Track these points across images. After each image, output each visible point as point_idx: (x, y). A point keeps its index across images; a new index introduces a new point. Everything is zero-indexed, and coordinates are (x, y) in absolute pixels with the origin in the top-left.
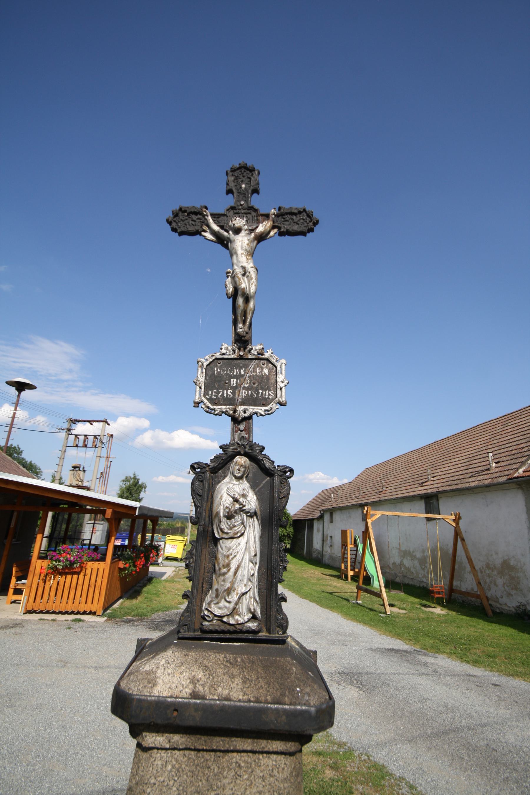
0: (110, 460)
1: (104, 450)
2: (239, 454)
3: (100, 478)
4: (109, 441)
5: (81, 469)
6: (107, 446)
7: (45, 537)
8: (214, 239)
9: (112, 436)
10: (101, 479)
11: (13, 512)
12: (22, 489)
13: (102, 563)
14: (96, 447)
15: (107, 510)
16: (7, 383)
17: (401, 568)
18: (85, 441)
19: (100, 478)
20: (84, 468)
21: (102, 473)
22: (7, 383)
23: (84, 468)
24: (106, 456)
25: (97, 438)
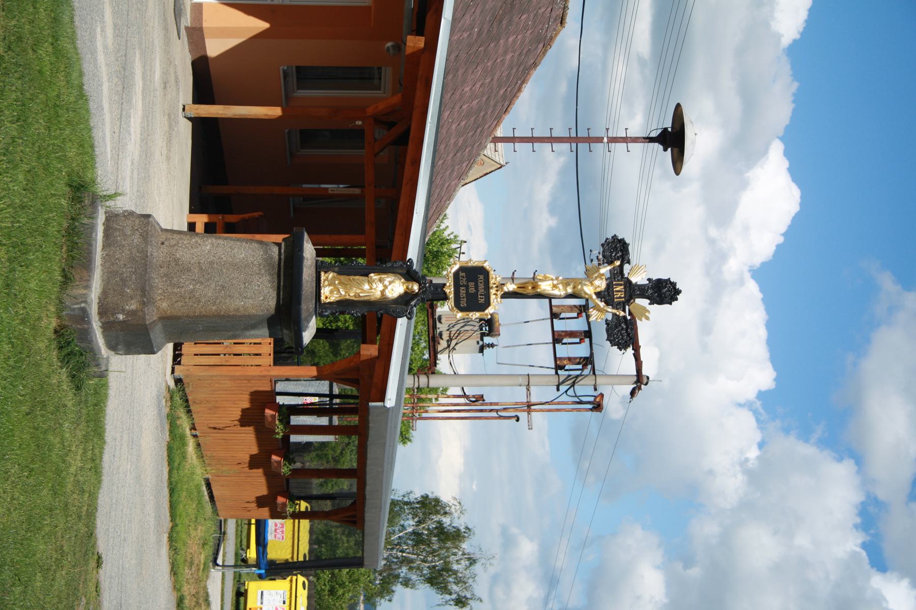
0: (523, 416)
1: (550, 393)
2: (420, 285)
3: (465, 396)
4: (581, 403)
5: (487, 340)
6: (564, 398)
7: (276, 570)
8: (264, 25)
9: (597, 406)
10: (462, 401)
11: (362, 187)
12: (405, 190)
13: (270, 360)
14: (558, 367)
15: (377, 346)
16: (678, 106)
17: (307, 498)
18: (571, 334)
19: (465, 396)
20: (492, 345)
21: (480, 398)
22: (678, 106)
23: (492, 345)
24: (534, 400)
25: (585, 366)
